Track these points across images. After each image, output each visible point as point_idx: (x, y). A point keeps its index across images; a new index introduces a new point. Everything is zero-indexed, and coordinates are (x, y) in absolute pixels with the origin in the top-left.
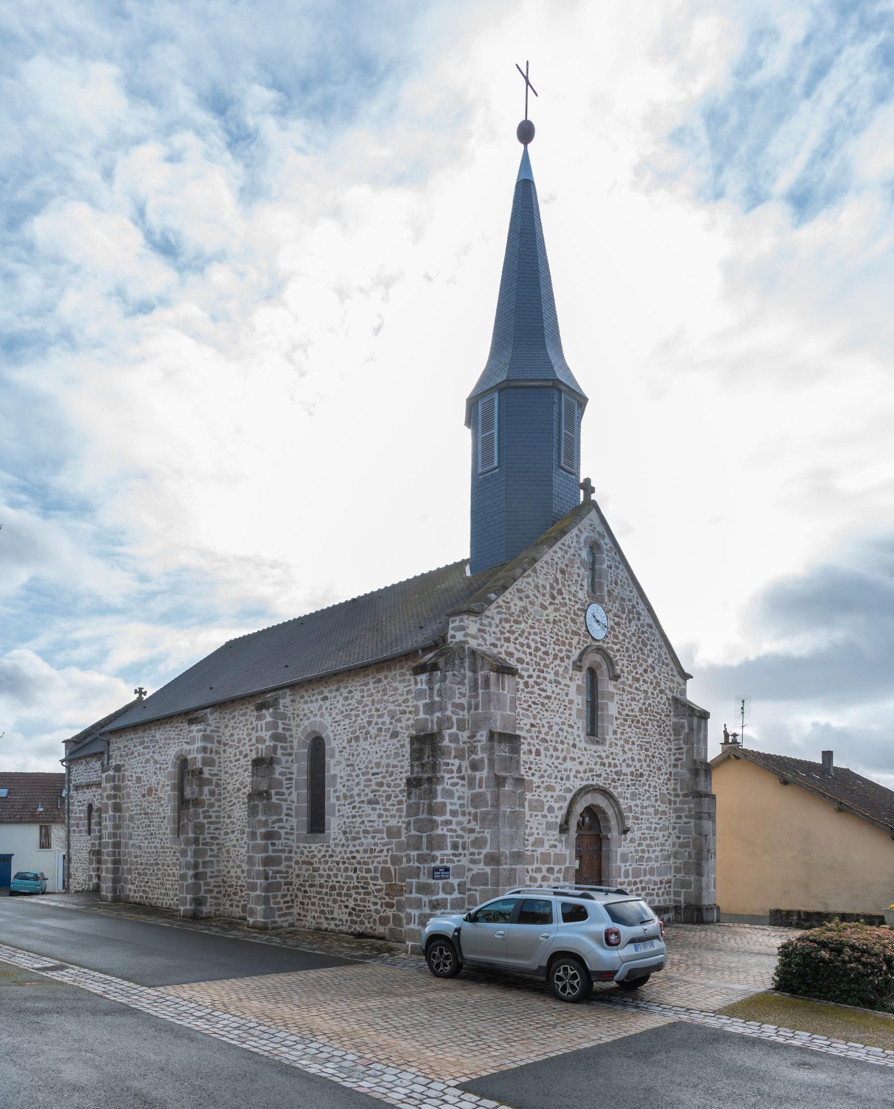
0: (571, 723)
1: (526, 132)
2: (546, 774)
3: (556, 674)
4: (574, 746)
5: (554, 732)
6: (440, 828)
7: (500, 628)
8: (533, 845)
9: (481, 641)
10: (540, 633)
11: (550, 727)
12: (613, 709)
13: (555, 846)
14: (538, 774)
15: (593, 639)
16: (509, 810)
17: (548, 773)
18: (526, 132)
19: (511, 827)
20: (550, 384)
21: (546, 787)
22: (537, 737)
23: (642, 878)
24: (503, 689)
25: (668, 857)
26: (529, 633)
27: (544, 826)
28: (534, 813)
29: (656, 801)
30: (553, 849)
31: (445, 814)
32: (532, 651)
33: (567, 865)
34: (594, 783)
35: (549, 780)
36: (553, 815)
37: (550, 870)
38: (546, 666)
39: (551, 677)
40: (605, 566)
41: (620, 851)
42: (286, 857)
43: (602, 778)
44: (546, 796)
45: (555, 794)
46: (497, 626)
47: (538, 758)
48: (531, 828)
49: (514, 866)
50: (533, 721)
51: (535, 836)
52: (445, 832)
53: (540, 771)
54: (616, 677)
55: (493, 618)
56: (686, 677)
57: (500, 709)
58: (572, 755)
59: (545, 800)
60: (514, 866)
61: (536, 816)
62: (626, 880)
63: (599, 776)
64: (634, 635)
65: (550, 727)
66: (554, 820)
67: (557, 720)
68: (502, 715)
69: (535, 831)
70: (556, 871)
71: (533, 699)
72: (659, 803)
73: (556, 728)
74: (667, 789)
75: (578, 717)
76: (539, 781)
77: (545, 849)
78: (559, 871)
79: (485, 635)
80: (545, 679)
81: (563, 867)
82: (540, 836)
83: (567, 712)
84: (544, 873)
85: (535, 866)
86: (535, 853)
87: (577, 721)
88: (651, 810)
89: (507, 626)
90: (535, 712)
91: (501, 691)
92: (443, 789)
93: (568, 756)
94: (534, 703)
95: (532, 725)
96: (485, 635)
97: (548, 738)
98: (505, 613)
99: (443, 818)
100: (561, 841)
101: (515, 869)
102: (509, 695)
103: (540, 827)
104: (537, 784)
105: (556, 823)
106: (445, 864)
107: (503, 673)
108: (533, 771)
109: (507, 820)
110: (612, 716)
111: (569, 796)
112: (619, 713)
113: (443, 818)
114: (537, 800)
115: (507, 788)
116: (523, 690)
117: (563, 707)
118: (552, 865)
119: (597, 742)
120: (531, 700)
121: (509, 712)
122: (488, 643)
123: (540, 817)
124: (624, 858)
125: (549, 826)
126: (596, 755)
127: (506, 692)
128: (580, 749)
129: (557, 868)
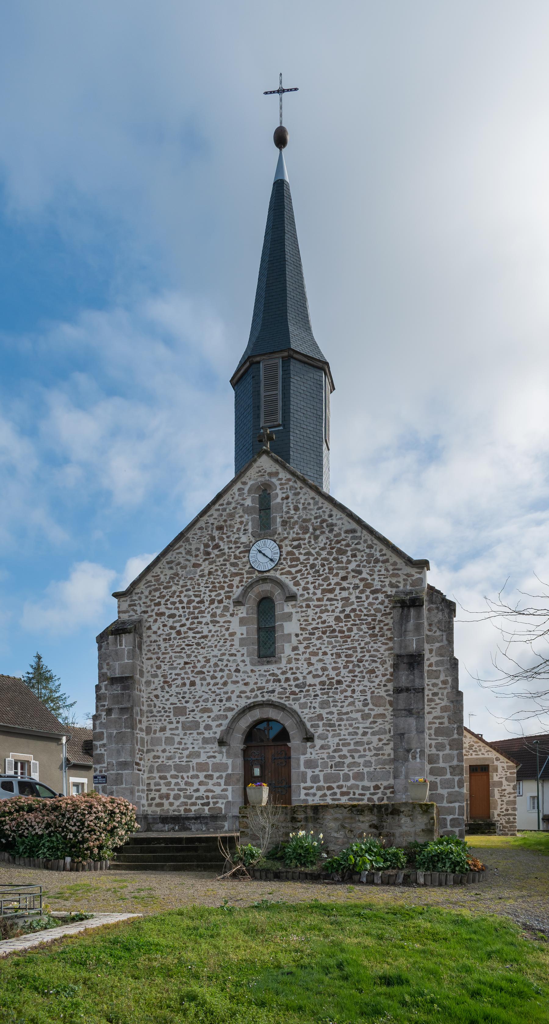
0: (233, 651)
1: (280, 139)
2: (201, 700)
3: (214, 615)
4: (237, 671)
5: (212, 663)
6: (99, 749)
7: (150, 597)
8: (187, 757)
9: (132, 613)
10: (194, 588)
11: (208, 661)
12: (291, 627)
13: (214, 757)
14: (192, 701)
15: (260, 572)
16: (115, 732)
17: (203, 698)
18: (280, 139)
19: (117, 743)
20: (248, 364)
21: (201, 710)
22: (192, 671)
23: (341, 783)
24: (121, 645)
25: (384, 763)
26: (181, 592)
27: (200, 742)
28: (188, 732)
29: (365, 705)
30: (212, 759)
31: (103, 740)
32: (185, 605)
33: (230, 771)
34: (264, 699)
35: (204, 704)
36: (211, 732)
37: (210, 777)
38: (202, 612)
39: (208, 618)
40: (279, 500)
41: (302, 758)
42: (362, 780)
43: (276, 693)
44: (201, 717)
45: (213, 715)
46: (147, 597)
47: (193, 688)
48: (185, 744)
49: (120, 772)
50: (186, 660)
51: (190, 749)
52: (103, 752)
53: (194, 698)
54: (292, 597)
55: (142, 593)
56: (423, 565)
57: (118, 660)
58: (234, 679)
59: (200, 720)
60: (120, 772)
61: (190, 734)
62: (315, 785)
63: (273, 691)
64: (323, 549)
65: (208, 661)
66: (212, 735)
67: (216, 652)
68: (120, 665)
69: (190, 746)
70: (215, 777)
71: (187, 642)
72: (371, 706)
73: (213, 661)
74: (387, 691)
75: (241, 645)
76: (194, 706)
77: (203, 759)
78: (220, 777)
79: (135, 608)
80: (200, 623)
81: (224, 774)
82: (196, 749)
83: (228, 644)
84: (202, 778)
85: (191, 773)
86: (190, 763)
87: (240, 649)
88: (358, 715)
89: (157, 594)
90: (189, 652)
91: (119, 647)
92: (101, 723)
93: (229, 681)
94: (187, 645)
95: (186, 663)
96: (135, 608)
97: (204, 670)
98: (155, 585)
99: (101, 742)
100: (221, 752)
101: (122, 774)
102: (126, 649)
103: (196, 742)
104: (191, 709)
105: (215, 738)
106: (103, 773)
107: (119, 634)
108: (187, 699)
109: (113, 739)
110: (290, 635)
111: (230, 715)
112: (302, 629)
113: (101, 742)
114: (192, 721)
115: (113, 716)
116: (175, 638)
117: (222, 641)
118: (210, 773)
119: (276, 662)
120: (184, 644)
121: (126, 661)
122: (139, 612)
123: (195, 735)
124: (310, 764)
125: (206, 741)
126: (267, 673)
127: (123, 647)
128: (245, 672)
129: (216, 775)
